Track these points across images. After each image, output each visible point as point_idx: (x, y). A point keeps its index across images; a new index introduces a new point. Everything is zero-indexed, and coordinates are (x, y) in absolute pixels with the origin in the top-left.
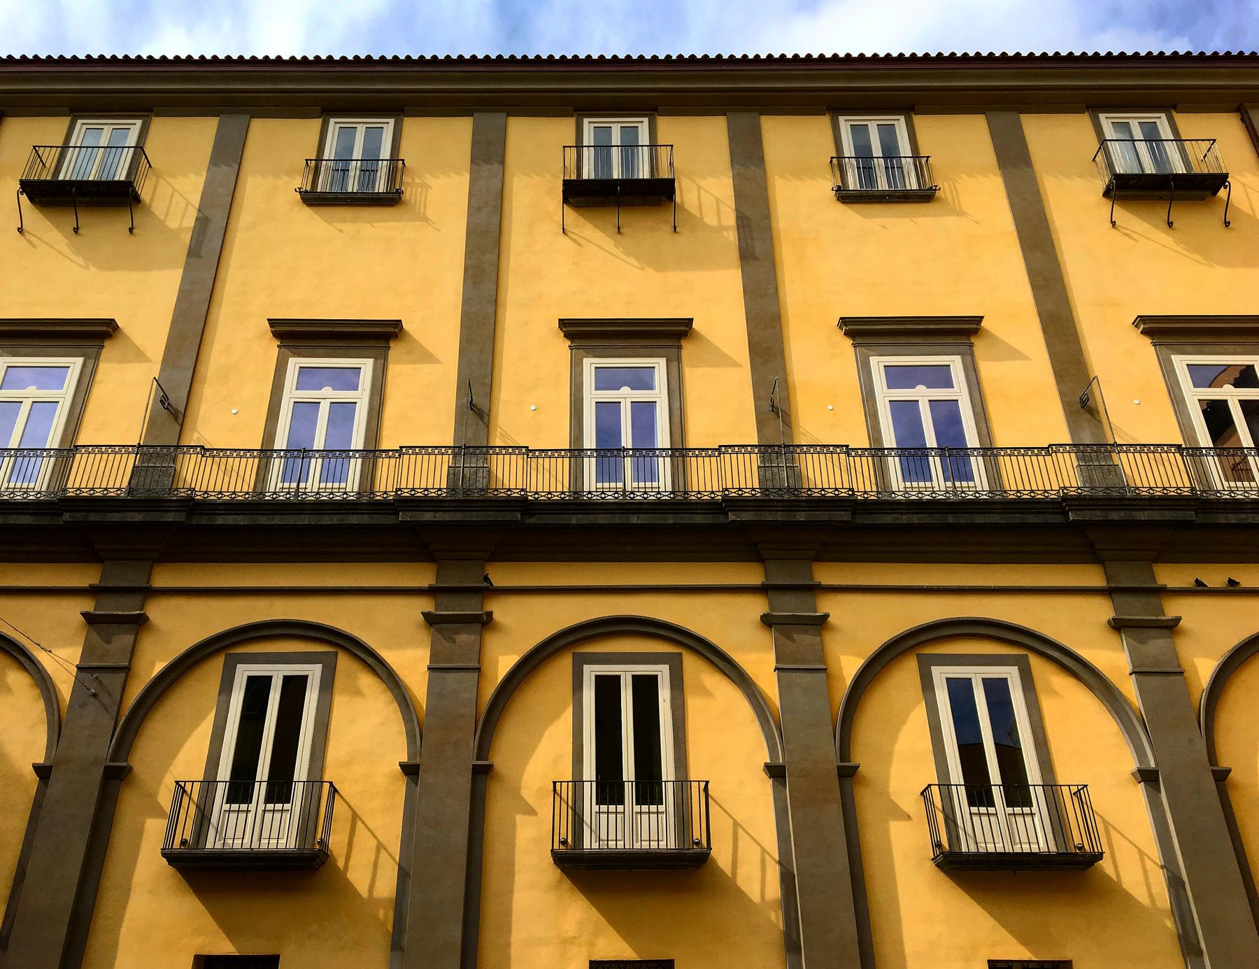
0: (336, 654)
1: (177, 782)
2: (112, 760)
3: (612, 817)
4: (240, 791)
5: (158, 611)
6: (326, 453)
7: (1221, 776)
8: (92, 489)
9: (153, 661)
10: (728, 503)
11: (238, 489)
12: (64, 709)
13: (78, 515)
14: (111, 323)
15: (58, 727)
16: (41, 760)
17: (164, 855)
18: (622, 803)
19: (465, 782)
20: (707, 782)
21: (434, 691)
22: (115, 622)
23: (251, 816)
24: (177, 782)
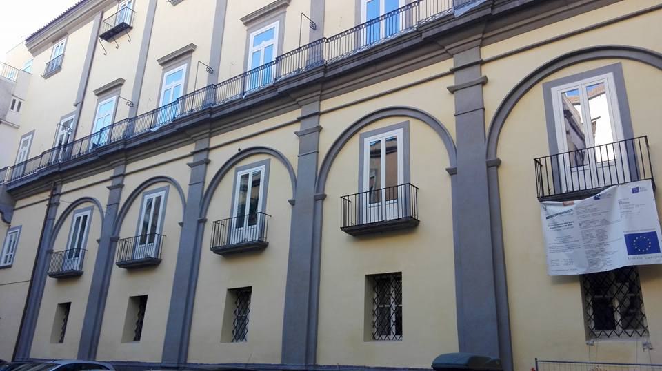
0: (169, 186)
1: (535, 159)
2: (317, 193)
3: (392, 205)
4: (240, 224)
5: (324, 121)
6: (387, 15)
7: (494, 164)
8: (434, 16)
9: (493, 98)
10: (299, 75)
11: (428, 16)
12: (455, 139)
13: (435, 30)
14: (120, 79)
15: (453, 149)
16: (448, 166)
17: (211, 250)
18: (243, 226)
19: (195, 224)
20: (646, 137)
21: (190, 193)
22: (470, 84)
23: (380, 208)
24: (535, 159)
